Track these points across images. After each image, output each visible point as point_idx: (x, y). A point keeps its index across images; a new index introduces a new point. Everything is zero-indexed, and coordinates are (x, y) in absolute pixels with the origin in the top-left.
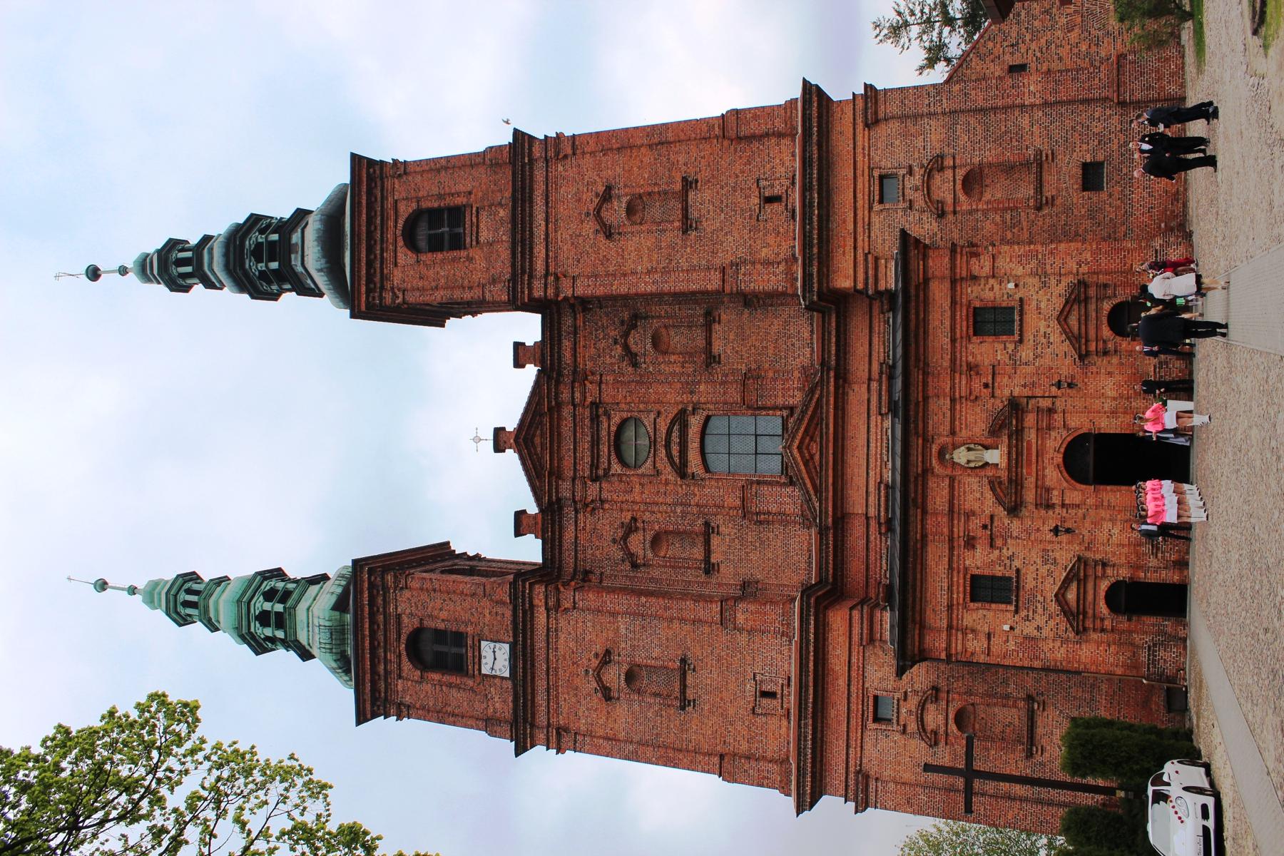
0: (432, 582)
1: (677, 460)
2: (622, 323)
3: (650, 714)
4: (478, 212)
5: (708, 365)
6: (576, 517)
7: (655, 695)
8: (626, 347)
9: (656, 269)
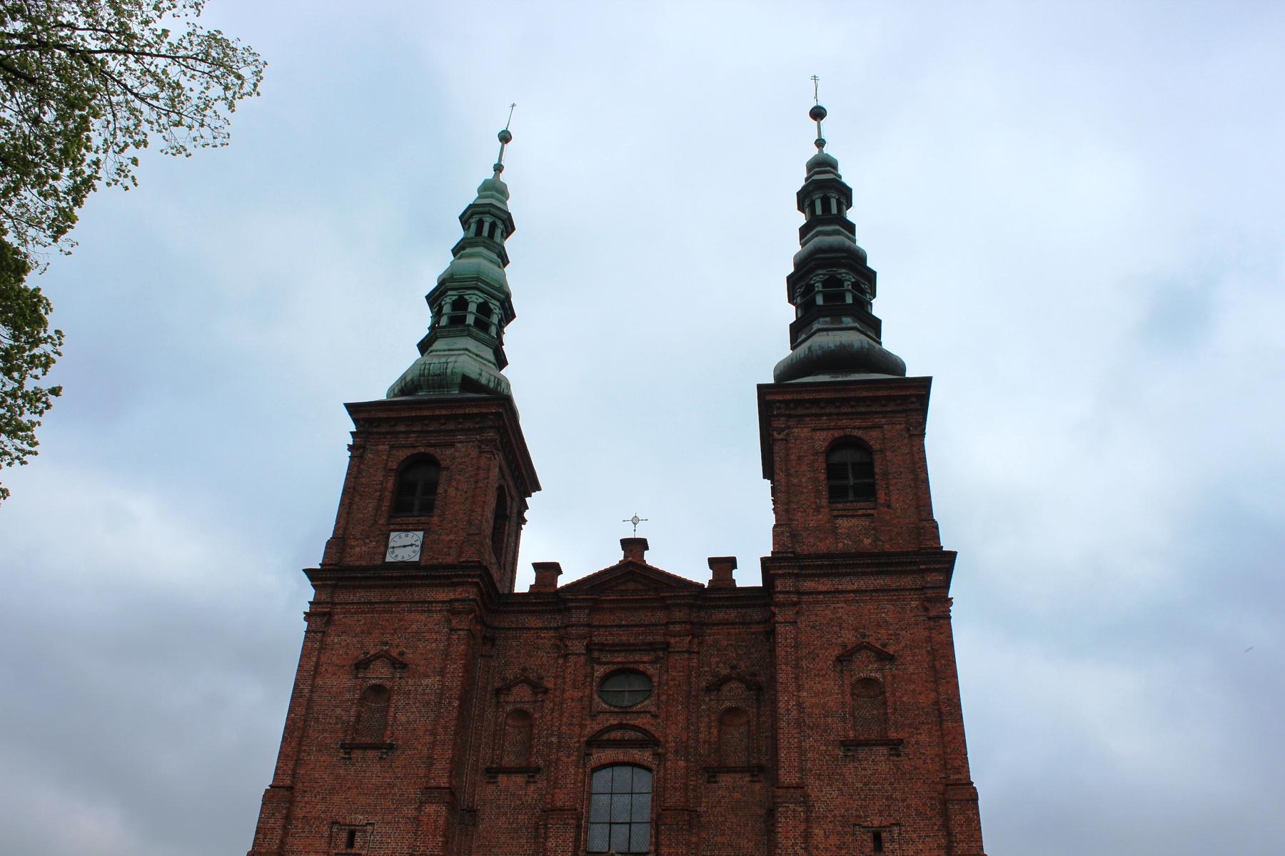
0: (484, 479)
1: (605, 737)
2: (753, 675)
3: (338, 711)
4: (868, 515)
5: (706, 769)
6: (551, 628)
7: (358, 716)
8: (727, 679)
9: (803, 712)
